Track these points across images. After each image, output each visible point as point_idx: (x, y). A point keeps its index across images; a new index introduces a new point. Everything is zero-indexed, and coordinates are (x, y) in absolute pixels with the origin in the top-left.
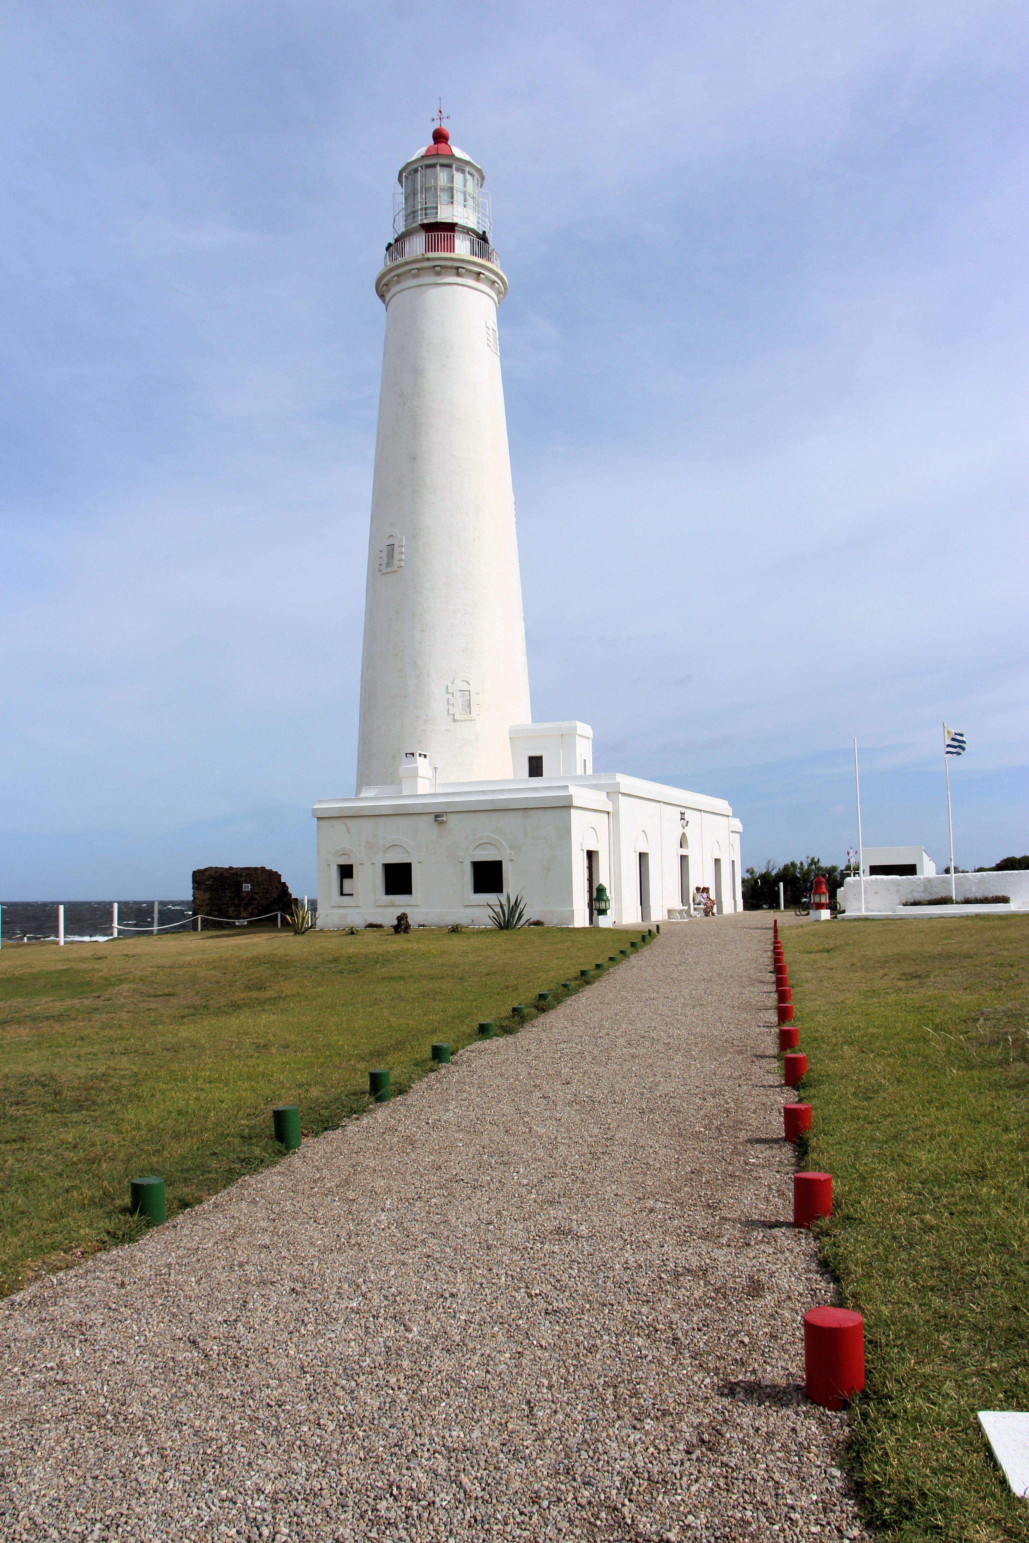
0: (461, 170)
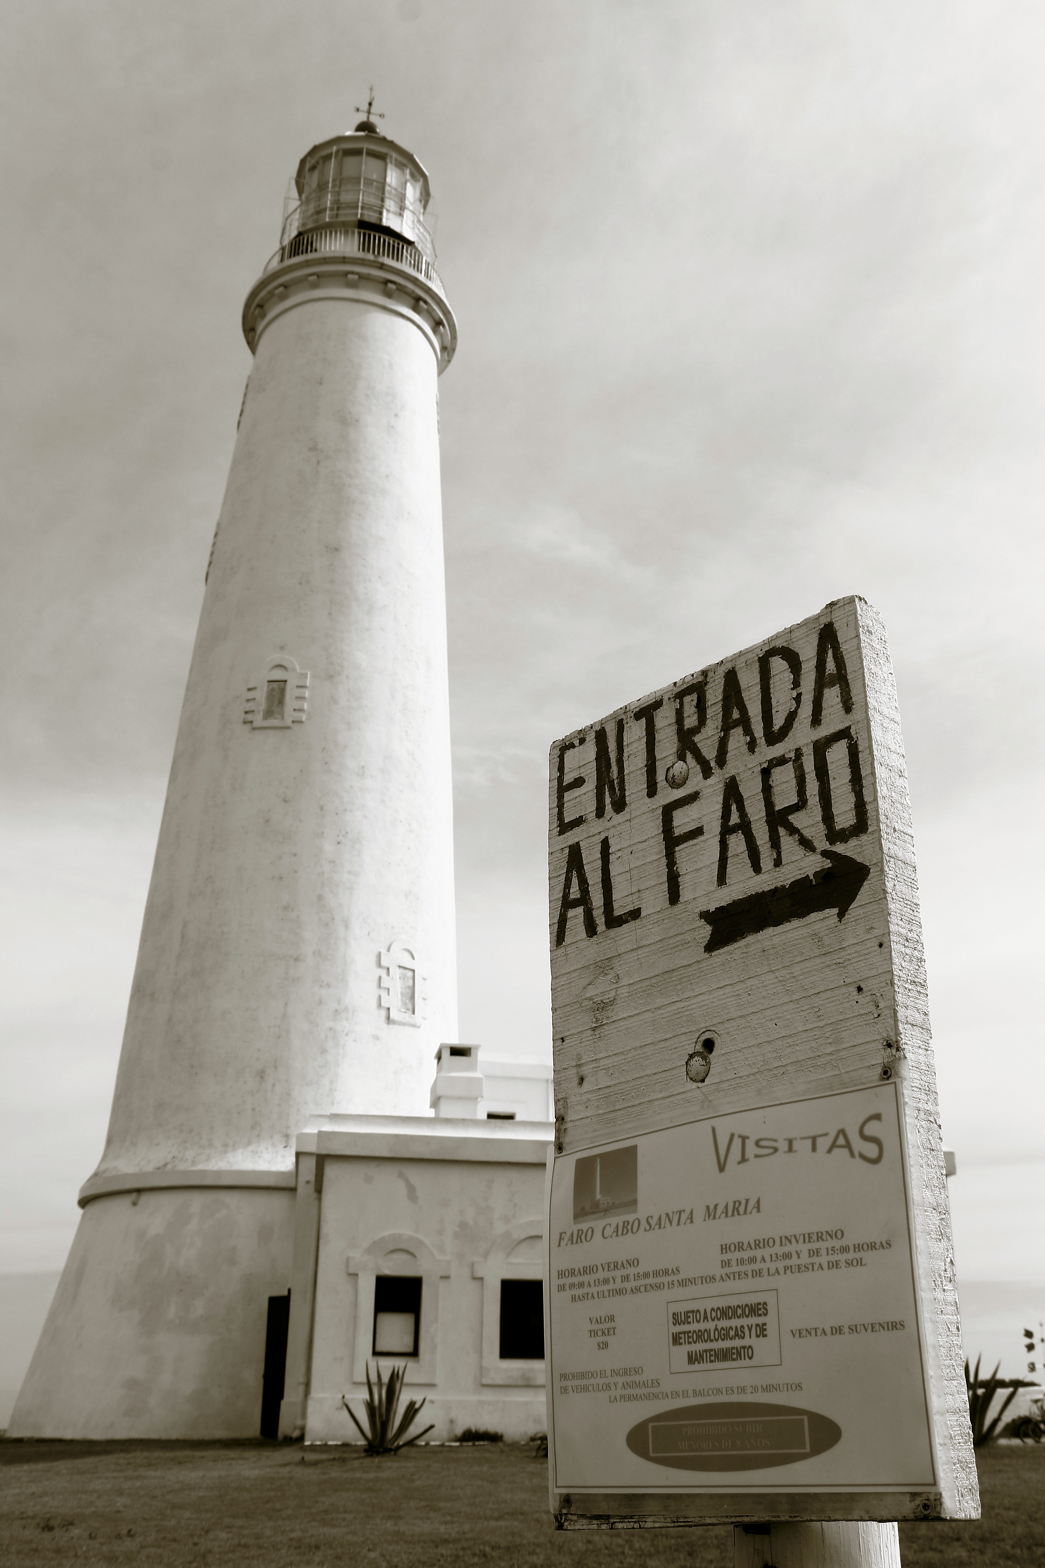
0: (400, 166)
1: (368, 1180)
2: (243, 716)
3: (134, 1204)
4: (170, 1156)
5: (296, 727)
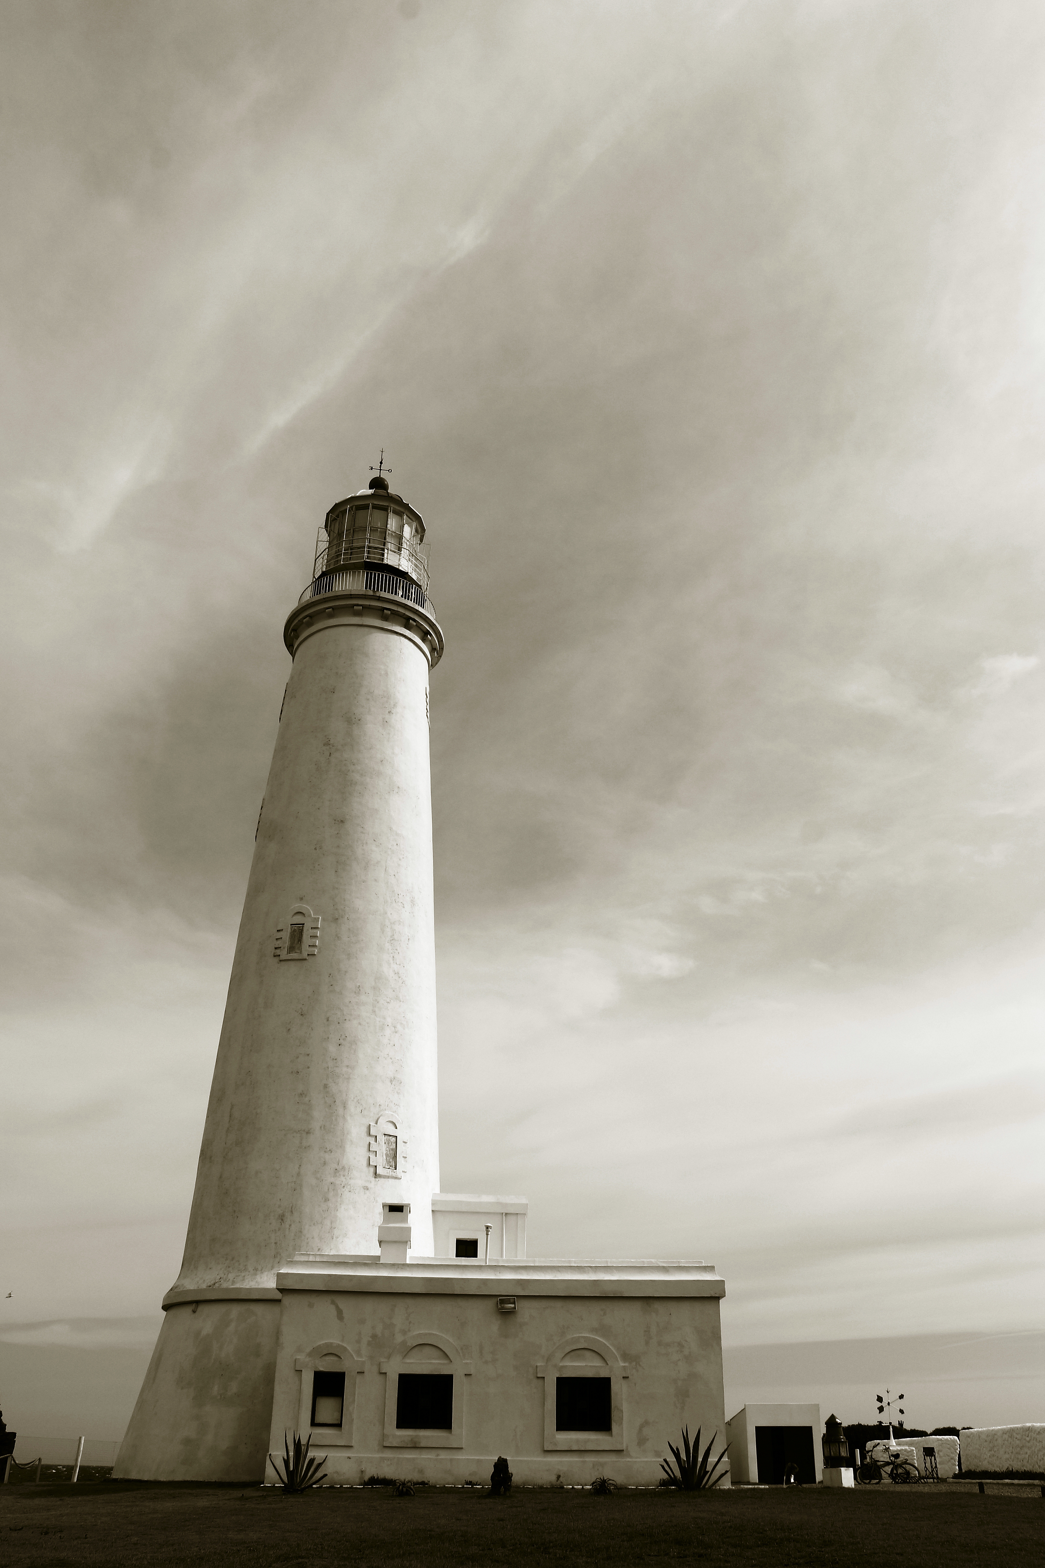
0: (399, 514)
1: (311, 1306)
2: (274, 950)
3: (194, 1312)
4: (218, 1277)
5: (311, 959)
